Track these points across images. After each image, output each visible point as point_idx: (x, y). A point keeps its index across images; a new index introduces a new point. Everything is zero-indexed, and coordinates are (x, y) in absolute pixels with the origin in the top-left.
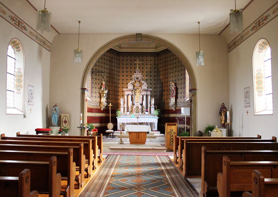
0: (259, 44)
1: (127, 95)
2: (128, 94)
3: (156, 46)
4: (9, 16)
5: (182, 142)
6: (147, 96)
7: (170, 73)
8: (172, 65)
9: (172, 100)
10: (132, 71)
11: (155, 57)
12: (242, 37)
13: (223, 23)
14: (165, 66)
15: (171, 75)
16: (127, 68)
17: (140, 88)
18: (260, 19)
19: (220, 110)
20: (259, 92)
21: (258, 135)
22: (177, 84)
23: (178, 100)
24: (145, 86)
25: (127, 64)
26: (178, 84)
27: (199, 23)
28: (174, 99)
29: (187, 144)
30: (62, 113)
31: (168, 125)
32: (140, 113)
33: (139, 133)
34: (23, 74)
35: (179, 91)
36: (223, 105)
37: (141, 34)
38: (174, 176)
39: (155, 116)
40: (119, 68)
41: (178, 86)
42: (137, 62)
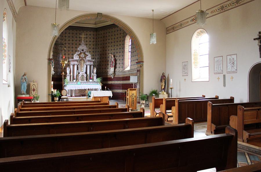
0: (197, 32)
1: (73, 64)
2: (74, 64)
3: (95, 22)
6: (90, 66)
7: (109, 46)
8: (111, 40)
9: (111, 69)
10: (74, 43)
11: (94, 32)
12: (181, 25)
13: (162, 13)
14: (104, 40)
15: (110, 48)
16: (69, 40)
17: (85, 59)
19: (161, 78)
20: (195, 65)
21: (203, 95)
22: (116, 56)
23: (117, 70)
24: (89, 57)
25: (69, 37)
26: (117, 56)
27: (153, 11)
28: (114, 69)
29: (179, 102)
30: (31, 82)
31: (130, 90)
32: (85, 81)
33: (103, 97)
34: (6, 44)
35: (118, 62)
36: (163, 74)
37: (102, 14)
39: (98, 83)
40: (62, 40)
41: (116, 58)
42: (83, 36)
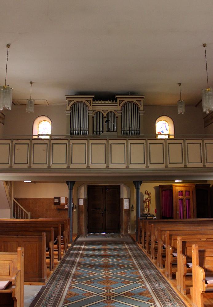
27: (180, 84)
38: (150, 274)
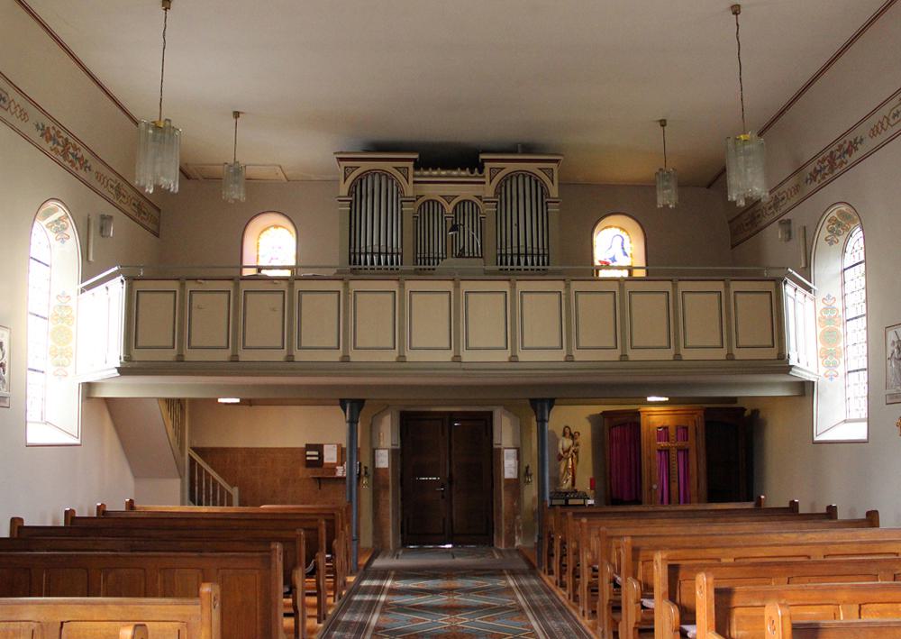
4: (37, 125)
5: (360, 263)
18: (833, 149)
27: (663, 123)
